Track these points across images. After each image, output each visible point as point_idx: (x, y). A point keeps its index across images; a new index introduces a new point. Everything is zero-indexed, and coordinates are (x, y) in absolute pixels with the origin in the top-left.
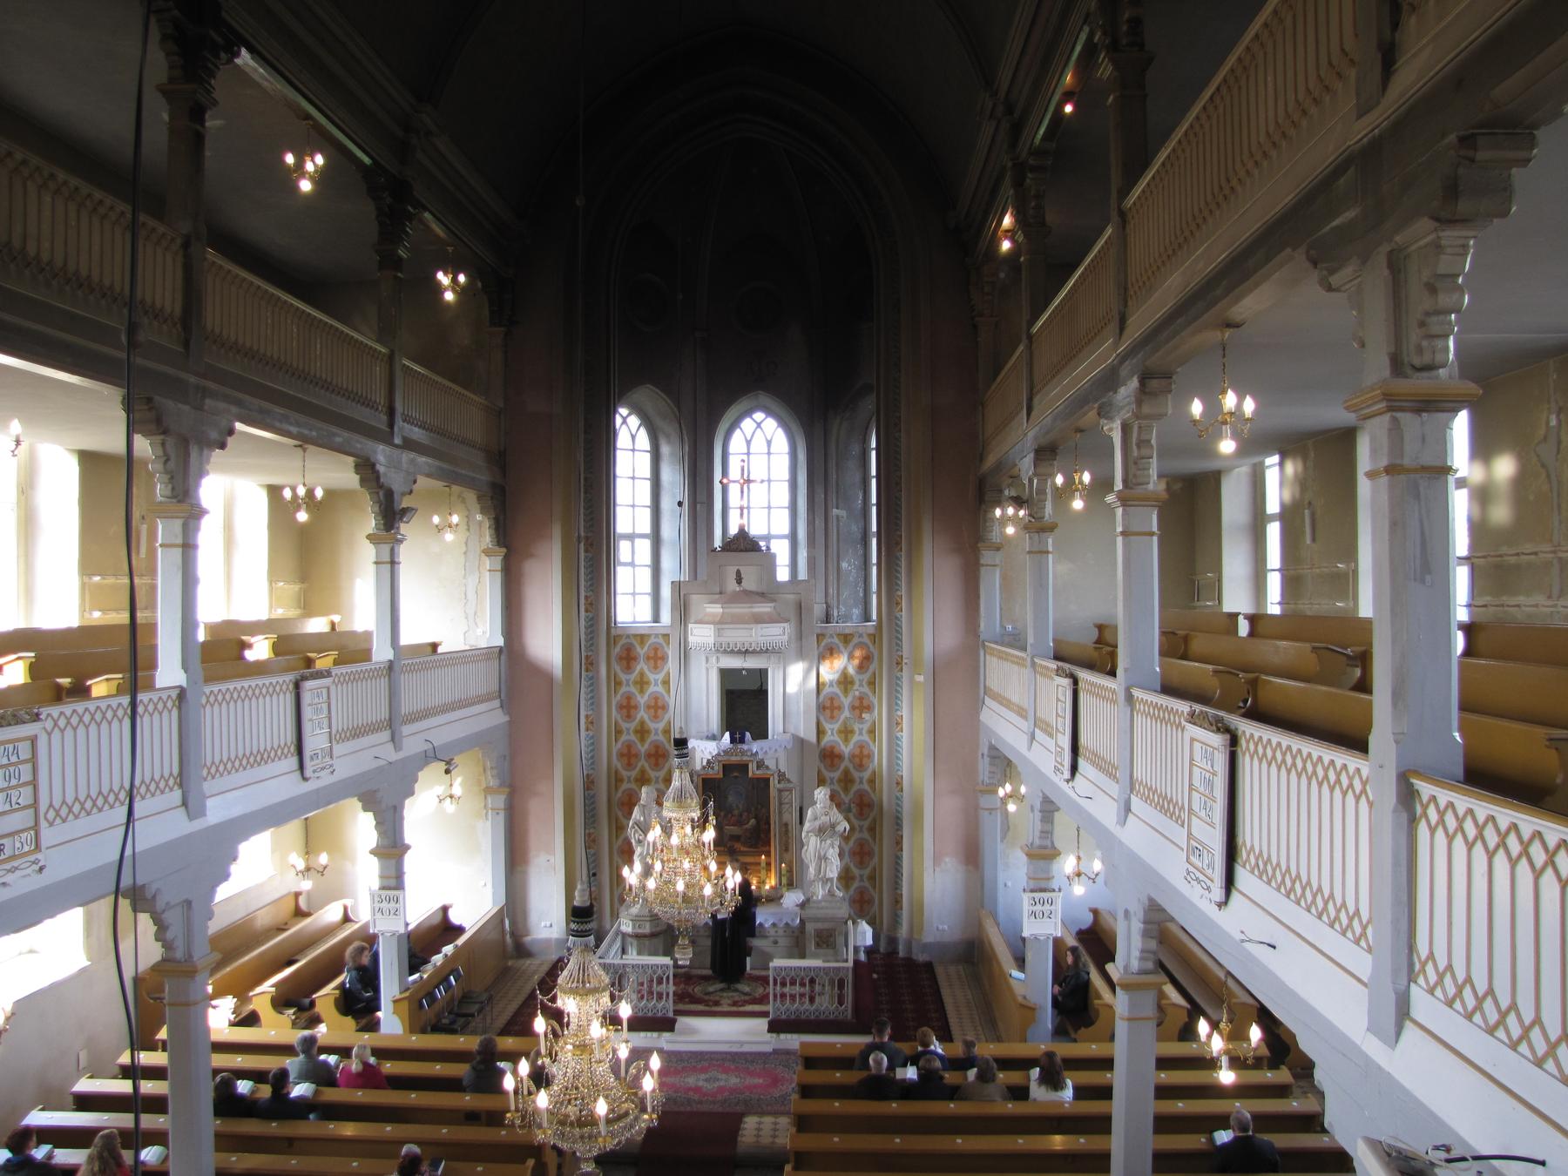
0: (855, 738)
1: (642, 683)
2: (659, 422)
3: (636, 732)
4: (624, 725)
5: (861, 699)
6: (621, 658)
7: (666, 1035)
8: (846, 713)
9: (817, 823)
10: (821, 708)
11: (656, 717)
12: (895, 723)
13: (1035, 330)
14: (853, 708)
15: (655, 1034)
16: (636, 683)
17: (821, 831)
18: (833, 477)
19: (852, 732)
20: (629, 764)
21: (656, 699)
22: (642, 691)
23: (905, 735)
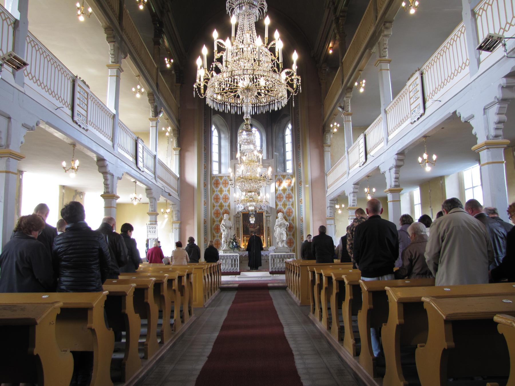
0: (288, 207)
1: (221, 191)
2: (220, 127)
3: (219, 206)
4: (215, 204)
5: (289, 195)
6: (215, 184)
7: (238, 276)
8: (284, 199)
9: (279, 223)
10: (277, 198)
11: (225, 202)
12: (300, 201)
13: (343, 60)
14: (286, 197)
15: (234, 276)
16: (219, 191)
17: (280, 226)
18: (274, 143)
19: (286, 205)
20: (217, 216)
21: (226, 196)
22: (221, 194)
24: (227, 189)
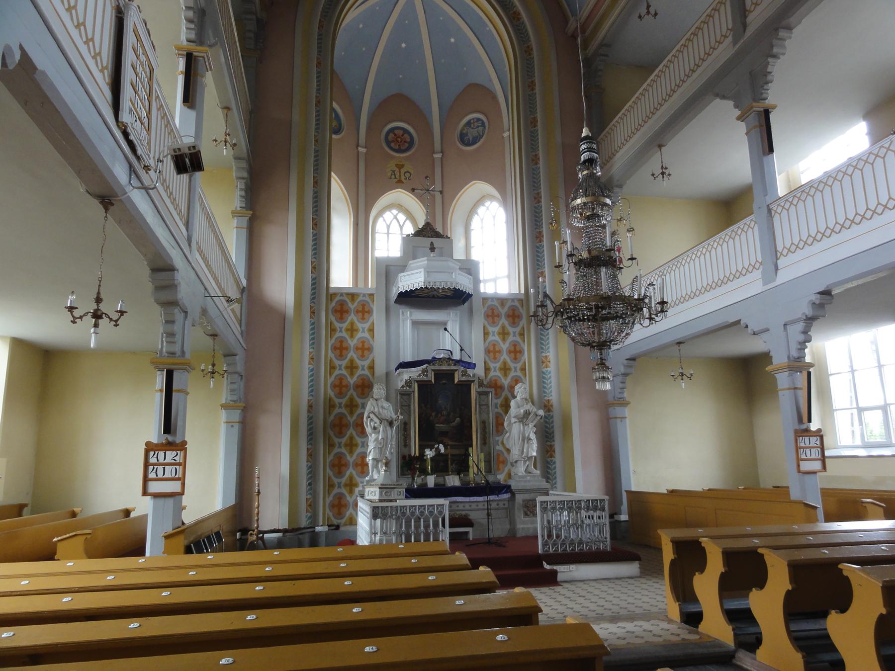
1: (352, 330)
10: (487, 351)
16: (347, 330)
20: (341, 355)
22: (352, 336)
23: (552, 368)
24: (367, 326)
